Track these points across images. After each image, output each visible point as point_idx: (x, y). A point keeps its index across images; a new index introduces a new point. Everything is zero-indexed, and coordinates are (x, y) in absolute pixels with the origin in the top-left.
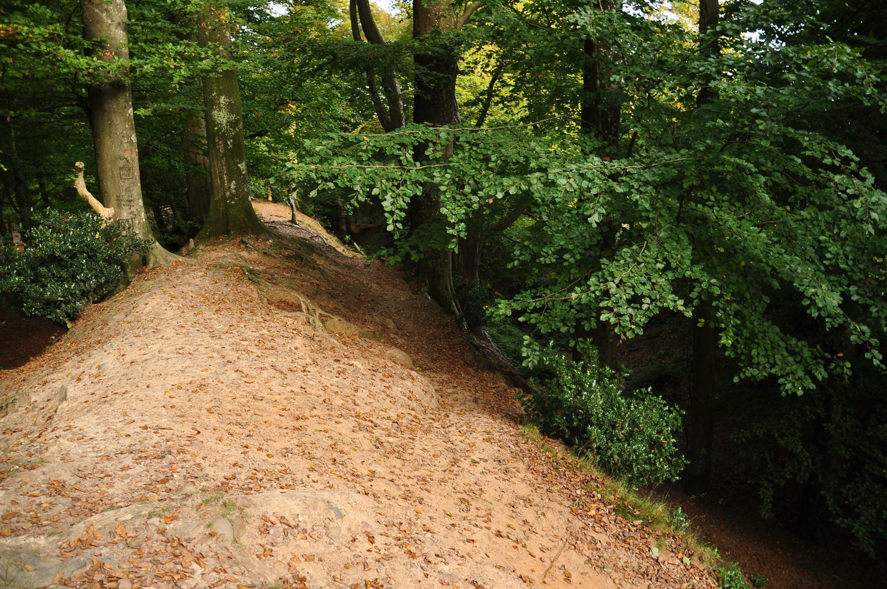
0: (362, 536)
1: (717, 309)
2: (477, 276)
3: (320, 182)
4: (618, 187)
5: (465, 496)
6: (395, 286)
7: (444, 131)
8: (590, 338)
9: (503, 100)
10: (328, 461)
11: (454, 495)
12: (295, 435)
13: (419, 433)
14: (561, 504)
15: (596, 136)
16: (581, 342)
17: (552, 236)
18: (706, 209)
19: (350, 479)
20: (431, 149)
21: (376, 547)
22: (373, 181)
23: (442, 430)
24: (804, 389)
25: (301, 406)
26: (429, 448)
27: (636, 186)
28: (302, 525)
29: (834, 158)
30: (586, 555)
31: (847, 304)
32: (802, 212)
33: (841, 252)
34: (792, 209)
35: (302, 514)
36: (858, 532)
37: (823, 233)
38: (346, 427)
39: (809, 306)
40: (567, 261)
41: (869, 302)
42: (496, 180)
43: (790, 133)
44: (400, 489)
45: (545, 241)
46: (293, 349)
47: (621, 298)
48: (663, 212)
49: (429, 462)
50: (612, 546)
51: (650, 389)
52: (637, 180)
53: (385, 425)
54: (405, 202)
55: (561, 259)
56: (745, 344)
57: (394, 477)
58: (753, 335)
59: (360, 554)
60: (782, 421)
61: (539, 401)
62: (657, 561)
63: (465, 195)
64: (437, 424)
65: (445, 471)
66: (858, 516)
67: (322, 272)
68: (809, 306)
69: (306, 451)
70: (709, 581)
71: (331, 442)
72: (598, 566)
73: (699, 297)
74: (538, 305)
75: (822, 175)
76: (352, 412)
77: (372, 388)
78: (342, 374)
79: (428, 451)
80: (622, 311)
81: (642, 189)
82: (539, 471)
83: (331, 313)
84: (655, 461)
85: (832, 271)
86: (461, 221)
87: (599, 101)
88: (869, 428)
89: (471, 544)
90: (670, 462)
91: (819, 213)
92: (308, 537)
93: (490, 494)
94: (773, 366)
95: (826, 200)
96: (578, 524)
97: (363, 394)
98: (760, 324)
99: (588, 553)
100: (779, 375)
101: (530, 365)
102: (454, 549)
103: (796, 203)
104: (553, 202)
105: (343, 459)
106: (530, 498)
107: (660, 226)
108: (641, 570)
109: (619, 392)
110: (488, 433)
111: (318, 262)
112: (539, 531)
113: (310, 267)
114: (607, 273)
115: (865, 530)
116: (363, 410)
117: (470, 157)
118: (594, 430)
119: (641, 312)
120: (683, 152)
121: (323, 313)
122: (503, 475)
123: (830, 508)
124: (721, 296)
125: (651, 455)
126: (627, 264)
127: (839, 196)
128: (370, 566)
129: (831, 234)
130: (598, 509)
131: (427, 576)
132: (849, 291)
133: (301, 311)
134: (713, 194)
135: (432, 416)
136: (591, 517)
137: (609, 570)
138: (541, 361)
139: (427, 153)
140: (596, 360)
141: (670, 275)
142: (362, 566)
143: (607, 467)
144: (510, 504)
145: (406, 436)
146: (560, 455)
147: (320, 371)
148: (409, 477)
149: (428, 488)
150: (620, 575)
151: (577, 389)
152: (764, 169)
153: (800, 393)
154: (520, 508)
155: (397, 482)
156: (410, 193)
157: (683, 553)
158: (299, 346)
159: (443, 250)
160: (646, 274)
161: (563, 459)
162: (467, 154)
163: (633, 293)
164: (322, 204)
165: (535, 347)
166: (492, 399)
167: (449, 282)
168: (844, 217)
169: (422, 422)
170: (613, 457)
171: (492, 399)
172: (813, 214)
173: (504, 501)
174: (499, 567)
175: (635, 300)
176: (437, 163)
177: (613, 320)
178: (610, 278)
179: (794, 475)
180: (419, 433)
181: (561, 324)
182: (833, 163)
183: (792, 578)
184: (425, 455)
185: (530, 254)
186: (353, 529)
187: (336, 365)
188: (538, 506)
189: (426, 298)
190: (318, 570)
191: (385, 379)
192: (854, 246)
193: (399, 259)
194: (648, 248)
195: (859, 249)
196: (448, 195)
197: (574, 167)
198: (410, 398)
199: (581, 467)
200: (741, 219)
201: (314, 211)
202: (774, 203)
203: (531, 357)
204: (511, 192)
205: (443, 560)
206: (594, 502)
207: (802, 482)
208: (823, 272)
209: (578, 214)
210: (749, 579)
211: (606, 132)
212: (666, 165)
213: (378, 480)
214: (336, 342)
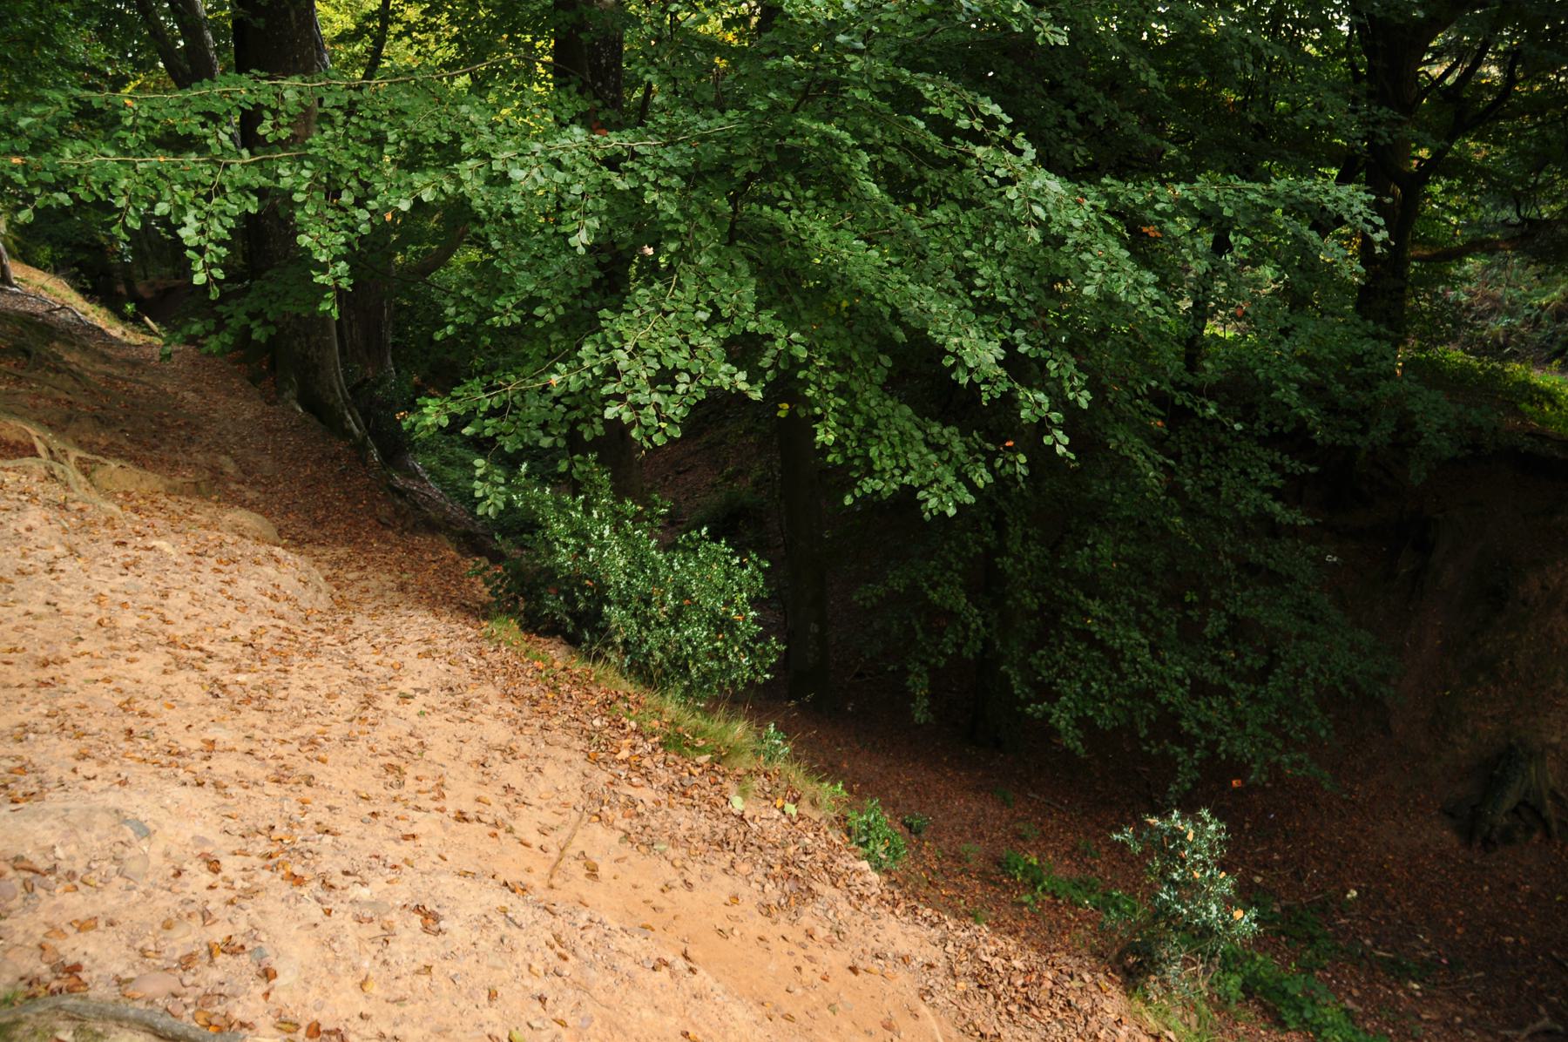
0: (195, 864)
1: (805, 383)
2: (390, 362)
3: (37, 191)
4: (619, 180)
5: (393, 760)
6: (231, 393)
7: (292, 87)
8: (593, 452)
9: (410, 29)
10: (116, 735)
11: (371, 761)
12: (40, 697)
13: (297, 659)
14: (568, 748)
15: (580, 91)
16: (578, 461)
17: (511, 276)
18: (778, 214)
19: (164, 762)
20: (268, 123)
21: (224, 879)
22: (154, 187)
23: (341, 650)
24: (958, 505)
25: (49, 638)
26: (318, 682)
27: (652, 178)
28: (65, 866)
29: (972, 118)
30: (620, 829)
31: (1012, 361)
32: (934, 212)
33: (998, 275)
34: (920, 208)
35: (62, 845)
36: (1058, 722)
37: (968, 246)
38: (149, 667)
39: (953, 368)
40: (541, 318)
41: (1045, 354)
42: (399, 178)
43: (904, 77)
44: (267, 766)
45: (499, 285)
46: (22, 530)
47: (638, 377)
48: (702, 221)
49: (320, 709)
50: (664, 806)
51: (704, 531)
52: (654, 167)
53: (228, 652)
54: (224, 227)
55: (529, 317)
56: (859, 440)
57: (253, 745)
58: (871, 424)
59: (192, 897)
60: (933, 563)
61: (517, 574)
62: (741, 818)
63: (343, 209)
64: (330, 637)
65: (351, 720)
66: (1058, 695)
67: (77, 377)
68: (953, 368)
69: (68, 724)
70: (831, 836)
71: (119, 699)
72: (642, 844)
73: (774, 366)
74: (496, 403)
75: (958, 147)
76: (160, 637)
77: (197, 587)
78: (132, 568)
79: (316, 689)
80: (641, 398)
81: (663, 182)
82: (524, 697)
83: (102, 455)
84: (725, 652)
85: (985, 307)
86: (337, 258)
87: (582, 28)
88: (1062, 557)
89: (410, 844)
90: (752, 651)
91: (960, 212)
92: (81, 886)
93: (440, 748)
94: (905, 472)
95: (972, 192)
96: (601, 777)
97: (179, 600)
98: (879, 405)
99: (623, 824)
100: (917, 485)
101: (491, 511)
102: (377, 857)
103: (925, 198)
104: (509, 214)
105: (147, 727)
106: (513, 745)
107: (699, 248)
108: (717, 838)
109: (654, 542)
110: (427, 642)
111: (66, 358)
112: (535, 801)
113: (49, 369)
114: (610, 335)
115: (1067, 716)
116: (179, 631)
117: (346, 134)
118: (614, 613)
119: (674, 398)
120: (731, 114)
121: (83, 455)
122: (459, 713)
123: (1016, 692)
124: (810, 360)
125: (719, 644)
126: (645, 316)
127: (985, 181)
128: (216, 916)
129: (981, 246)
130: (634, 747)
131: (328, 913)
132: (1013, 338)
133: (38, 456)
134: (787, 187)
135: (320, 625)
136: (623, 762)
137: (662, 847)
138: (509, 503)
139: (261, 131)
140: (606, 491)
141: (722, 331)
142: (200, 918)
143: (643, 673)
144: (477, 761)
145: (273, 666)
146: (559, 664)
147: (86, 567)
148: (284, 742)
149: (322, 755)
150: (682, 852)
151: (577, 545)
152: (870, 141)
153: (951, 512)
154: (497, 764)
155: (259, 754)
156: (234, 209)
157: (784, 799)
158: (34, 523)
159: (313, 315)
160: (680, 332)
161: (565, 669)
162: (340, 131)
163: (658, 367)
164: (67, 244)
165: (496, 478)
166: (432, 582)
167: (336, 379)
168: (1000, 218)
169: (301, 639)
170: (652, 655)
171: (432, 582)
172: (951, 215)
173: (466, 757)
174: (465, 874)
175: (664, 378)
176: (285, 150)
177: (627, 417)
178: (616, 344)
179: (959, 646)
180: (297, 659)
181: (540, 433)
182: (972, 127)
183: (970, 810)
184: (312, 696)
185: (475, 312)
186: (173, 854)
187: (119, 553)
188: (526, 756)
189: (293, 410)
190: (106, 944)
191: (221, 567)
192: (1019, 266)
193: (227, 338)
194: (680, 286)
195: (1025, 269)
196: (310, 210)
197: (537, 147)
198: (274, 598)
199: (598, 679)
200: (836, 229)
201: (52, 259)
202: (886, 197)
203: (492, 497)
204: (425, 198)
205: (358, 879)
206: (626, 736)
207: (971, 656)
208: (973, 310)
209: (556, 234)
210: (903, 822)
211: (599, 84)
212: (704, 139)
213: (223, 755)
214: (116, 509)
